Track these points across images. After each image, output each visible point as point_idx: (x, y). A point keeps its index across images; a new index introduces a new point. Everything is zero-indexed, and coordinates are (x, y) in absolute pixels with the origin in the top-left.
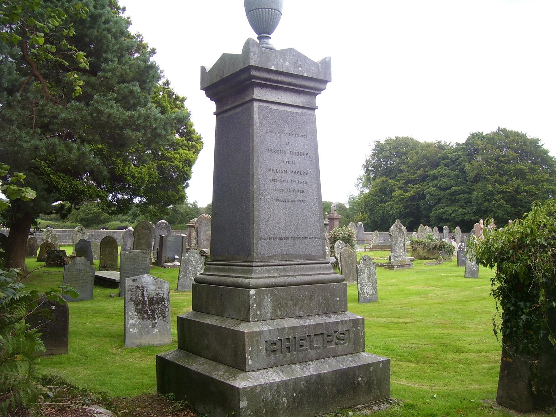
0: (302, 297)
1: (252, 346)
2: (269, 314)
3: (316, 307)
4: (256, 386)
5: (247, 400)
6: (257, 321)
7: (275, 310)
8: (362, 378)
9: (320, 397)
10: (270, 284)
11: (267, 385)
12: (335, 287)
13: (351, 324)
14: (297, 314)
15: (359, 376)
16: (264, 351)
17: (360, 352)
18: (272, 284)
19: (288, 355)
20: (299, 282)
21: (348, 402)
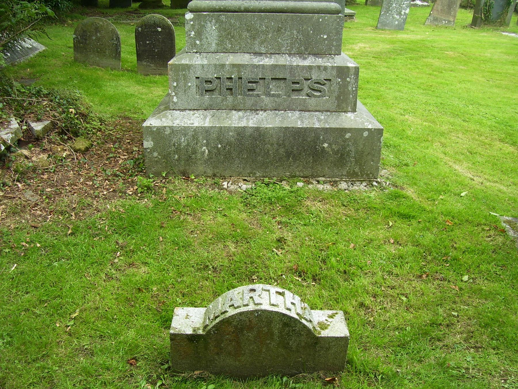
0: (265, 28)
1: (177, 81)
2: (214, 45)
3: (287, 43)
4: (165, 127)
5: (152, 140)
6: (197, 52)
7: (222, 41)
8: (330, 144)
9: (259, 156)
10: (217, 7)
11: (180, 129)
12: (321, 20)
13: (334, 73)
14: (257, 50)
15: (324, 141)
16: (194, 90)
17: (346, 112)
18: (220, 8)
19: (230, 98)
20: (263, 9)
21: (304, 170)
